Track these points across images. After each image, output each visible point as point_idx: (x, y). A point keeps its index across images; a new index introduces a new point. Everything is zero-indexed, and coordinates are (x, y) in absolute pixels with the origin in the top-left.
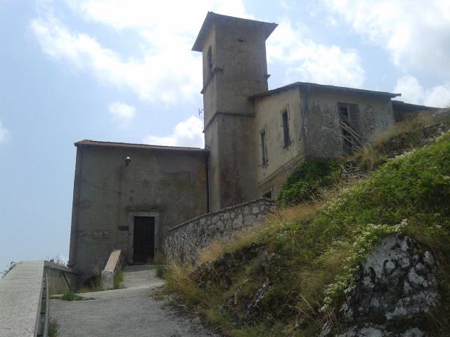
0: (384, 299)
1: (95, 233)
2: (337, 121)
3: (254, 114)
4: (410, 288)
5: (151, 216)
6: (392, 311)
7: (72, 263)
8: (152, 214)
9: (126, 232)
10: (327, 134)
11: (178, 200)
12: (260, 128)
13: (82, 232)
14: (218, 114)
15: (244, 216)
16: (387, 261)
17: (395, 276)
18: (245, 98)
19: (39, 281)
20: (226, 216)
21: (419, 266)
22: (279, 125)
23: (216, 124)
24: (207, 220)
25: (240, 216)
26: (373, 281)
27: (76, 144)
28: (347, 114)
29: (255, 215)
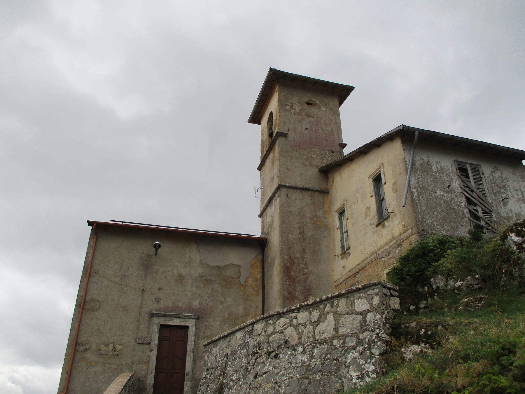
1: (102, 347)
2: (456, 184)
5: (183, 324)
8: (183, 323)
9: (147, 346)
11: (222, 303)
14: (280, 187)
15: (337, 317)
18: (317, 170)
19: (152, 379)
20: (302, 316)
22: (369, 196)
23: (277, 203)
24: (267, 325)
25: (330, 317)
28: (467, 177)
29: (361, 313)
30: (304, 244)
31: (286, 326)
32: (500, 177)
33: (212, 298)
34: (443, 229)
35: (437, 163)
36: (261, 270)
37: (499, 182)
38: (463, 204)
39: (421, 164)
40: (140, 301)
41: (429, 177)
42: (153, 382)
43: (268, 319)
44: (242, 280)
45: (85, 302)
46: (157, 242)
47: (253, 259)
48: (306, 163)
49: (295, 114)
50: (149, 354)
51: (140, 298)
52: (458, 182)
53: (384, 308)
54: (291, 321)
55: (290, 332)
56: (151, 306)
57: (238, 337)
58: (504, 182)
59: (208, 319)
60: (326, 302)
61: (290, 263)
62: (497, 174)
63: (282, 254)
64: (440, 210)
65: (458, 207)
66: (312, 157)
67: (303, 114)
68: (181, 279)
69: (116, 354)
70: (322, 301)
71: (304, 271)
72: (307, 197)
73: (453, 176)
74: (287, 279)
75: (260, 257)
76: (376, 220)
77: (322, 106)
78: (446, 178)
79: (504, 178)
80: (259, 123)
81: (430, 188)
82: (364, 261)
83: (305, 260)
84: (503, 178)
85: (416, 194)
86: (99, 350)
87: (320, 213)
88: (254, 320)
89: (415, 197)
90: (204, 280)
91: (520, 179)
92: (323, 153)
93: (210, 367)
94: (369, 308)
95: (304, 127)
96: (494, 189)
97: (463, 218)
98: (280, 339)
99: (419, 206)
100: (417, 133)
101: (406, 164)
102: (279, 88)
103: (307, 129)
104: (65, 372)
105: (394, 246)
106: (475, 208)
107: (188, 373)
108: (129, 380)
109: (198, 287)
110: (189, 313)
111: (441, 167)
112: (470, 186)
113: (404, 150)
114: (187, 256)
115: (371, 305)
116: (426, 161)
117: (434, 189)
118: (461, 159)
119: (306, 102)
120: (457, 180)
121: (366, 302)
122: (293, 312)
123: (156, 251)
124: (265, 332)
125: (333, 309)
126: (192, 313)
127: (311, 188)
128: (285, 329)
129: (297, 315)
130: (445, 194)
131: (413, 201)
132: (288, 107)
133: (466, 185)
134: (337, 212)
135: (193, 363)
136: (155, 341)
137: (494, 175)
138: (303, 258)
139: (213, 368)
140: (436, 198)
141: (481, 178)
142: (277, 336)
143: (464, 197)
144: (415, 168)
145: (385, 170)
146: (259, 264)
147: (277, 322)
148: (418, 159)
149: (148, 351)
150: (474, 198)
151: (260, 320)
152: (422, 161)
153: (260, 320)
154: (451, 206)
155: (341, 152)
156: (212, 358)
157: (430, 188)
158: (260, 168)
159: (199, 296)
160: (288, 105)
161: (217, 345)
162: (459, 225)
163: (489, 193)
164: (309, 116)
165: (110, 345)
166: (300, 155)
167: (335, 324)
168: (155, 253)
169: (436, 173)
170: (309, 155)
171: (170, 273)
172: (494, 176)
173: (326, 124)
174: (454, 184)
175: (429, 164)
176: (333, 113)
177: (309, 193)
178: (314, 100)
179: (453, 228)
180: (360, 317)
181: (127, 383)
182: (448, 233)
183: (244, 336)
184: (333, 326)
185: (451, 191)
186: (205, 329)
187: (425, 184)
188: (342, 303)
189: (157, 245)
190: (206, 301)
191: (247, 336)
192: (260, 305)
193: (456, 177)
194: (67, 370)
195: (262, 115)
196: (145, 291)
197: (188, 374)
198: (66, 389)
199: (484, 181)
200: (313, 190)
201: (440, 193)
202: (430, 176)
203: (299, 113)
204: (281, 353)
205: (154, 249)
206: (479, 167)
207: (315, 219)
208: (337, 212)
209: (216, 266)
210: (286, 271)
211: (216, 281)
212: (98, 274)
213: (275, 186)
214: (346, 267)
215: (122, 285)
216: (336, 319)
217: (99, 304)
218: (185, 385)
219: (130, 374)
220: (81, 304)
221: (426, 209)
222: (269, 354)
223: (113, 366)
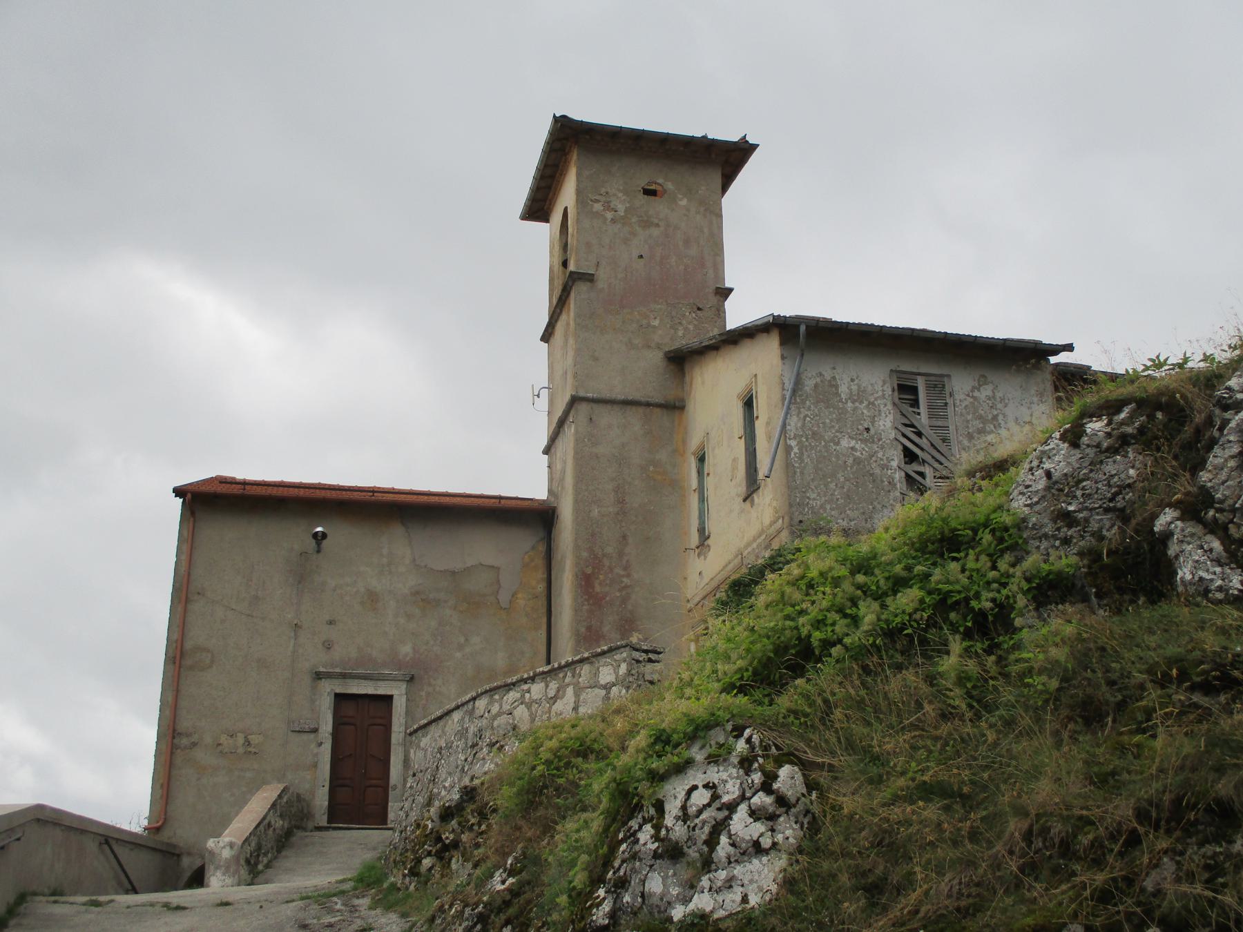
0: (675, 874)
1: (224, 739)
2: (887, 423)
3: (683, 400)
4: (731, 850)
5: (381, 692)
6: (686, 901)
7: (154, 829)
8: (382, 689)
9: (312, 736)
10: (857, 461)
11: (460, 647)
12: (694, 443)
13: (188, 735)
14: (574, 401)
16: (695, 788)
17: (704, 822)
18: (661, 355)
21: (760, 799)
23: (570, 431)
24: (491, 702)
25: (570, 691)
26: (656, 838)
27: (179, 492)
28: (915, 403)
30: (624, 524)
31: (516, 703)
32: (989, 399)
33: (439, 638)
34: (843, 516)
35: (852, 380)
36: (545, 576)
37: (986, 408)
38: (894, 464)
39: (816, 386)
40: (291, 648)
41: (830, 412)
42: (327, 803)
43: (492, 693)
44: (504, 597)
45: (182, 654)
46: (319, 529)
47: (526, 553)
48: (636, 341)
49: (613, 221)
50: (315, 751)
51: (292, 641)
52: (891, 417)
53: (631, 679)
54: (523, 696)
55: (521, 712)
56: (318, 659)
57: (456, 720)
58: (996, 409)
59: (432, 680)
60: (566, 669)
61: (593, 567)
62: (986, 391)
63: (577, 547)
64: (842, 479)
65: (883, 469)
66: (649, 325)
67: (634, 220)
68: (372, 601)
69: (250, 751)
70: (561, 668)
71: (622, 582)
72: (634, 419)
73: (882, 406)
74: (586, 600)
75: (542, 548)
76: (742, 489)
77: (680, 196)
78: (865, 411)
79: (999, 400)
80: (547, 221)
81: (828, 435)
82: (726, 565)
83: (626, 558)
84: (995, 400)
85: (796, 450)
86: (220, 744)
87: (662, 456)
88: (474, 694)
89: (792, 455)
90: (423, 600)
91: (1035, 399)
92: (677, 313)
93: (417, 769)
94: (614, 680)
95: (635, 254)
96: (970, 426)
97: (889, 491)
98: (508, 723)
99: (798, 474)
100: (803, 328)
101: (783, 389)
102: (578, 159)
103: (641, 257)
104: (158, 786)
105: (763, 546)
106: (921, 469)
107: (395, 785)
108: (280, 796)
109: (409, 617)
110: (392, 670)
111: (859, 386)
112: (916, 424)
113: (783, 358)
114: (385, 551)
115: (617, 674)
116: (829, 378)
117: (837, 437)
118: (907, 366)
119: (643, 188)
120: (890, 413)
121: (612, 671)
122: (526, 683)
123: (319, 544)
124: (489, 712)
125: (575, 680)
126: (399, 669)
127: (643, 400)
128: (515, 708)
129: (530, 688)
130: (857, 446)
131: (788, 465)
132: (598, 207)
133: (908, 423)
134: (694, 454)
135: (404, 766)
136: (327, 726)
137: (976, 394)
138: (621, 554)
139: (421, 771)
140: (837, 457)
141: (946, 404)
142: (503, 720)
143: (900, 447)
144: (800, 396)
145: (759, 390)
146: (540, 562)
147: (505, 698)
148: (810, 375)
149: (313, 746)
150: (922, 449)
151: (482, 694)
152: (818, 380)
153: (482, 694)
154: (868, 468)
155: (720, 313)
156: (420, 754)
157: (828, 435)
158: (547, 337)
159: (413, 634)
160: (597, 201)
161: (427, 733)
162: (879, 507)
163: (957, 433)
164: (647, 224)
165: (239, 734)
166: (623, 322)
167: (575, 702)
168: (316, 549)
169: (847, 403)
170: (644, 322)
171: (349, 588)
172: (975, 398)
173: (687, 242)
174: (881, 423)
175: (833, 384)
176: (705, 210)
177: (641, 410)
178: (660, 181)
179: (864, 513)
180: (603, 692)
181: (276, 800)
182: (853, 523)
183: (463, 719)
184: (572, 705)
185: (872, 437)
186: (427, 700)
187: (819, 427)
188: (586, 669)
189: (320, 534)
190: (428, 643)
191: (467, 719)
192: (543, 649)
193: (890, 406)
194: (161, 781)
195: (550, 204)
196: (300, 627)
197: (395, 787)
198: (163, 817)
199: (950, 409)
200: (648, 405)
201: (849, 442)
202: (832, 410)
203: (622, 218)
204: (507, 744)
205: (314, 541)
206: (946, 379)
207: (651, 468)
208: (694, 454)
209: (447, 570)
210: (583, 583)
211: (445, 602)
212: (203, 595)
213: (567, 398)
214: (704, 573)
215: (252, 616)
216: (577, 695)
217: (209, 655)
218: (389, 809)
219: (281, 787)
220: (175, 658)
221: (813, 480)
222: (491, 745)
223: (248, 775)
